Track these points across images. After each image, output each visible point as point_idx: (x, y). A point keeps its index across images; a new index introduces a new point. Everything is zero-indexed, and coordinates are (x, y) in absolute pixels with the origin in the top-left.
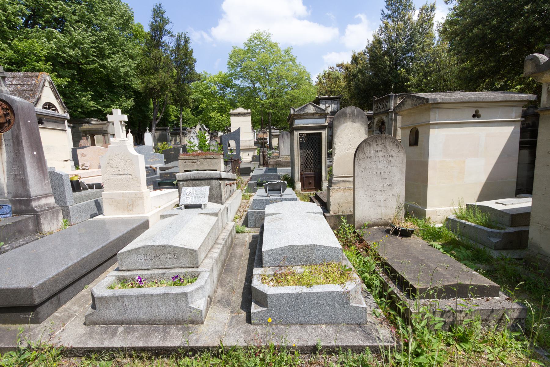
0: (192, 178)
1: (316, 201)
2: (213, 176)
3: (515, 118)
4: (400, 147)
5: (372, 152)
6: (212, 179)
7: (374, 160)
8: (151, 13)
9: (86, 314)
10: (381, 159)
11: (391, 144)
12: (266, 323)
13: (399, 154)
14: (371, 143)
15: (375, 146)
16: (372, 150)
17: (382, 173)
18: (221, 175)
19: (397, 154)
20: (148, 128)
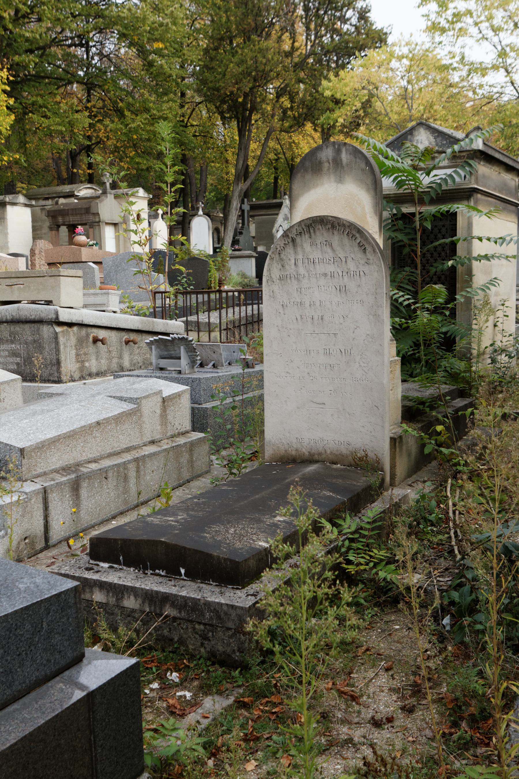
0: (9, 318)
1: (204, 258)
2: (43, 315)
3: (500, 192)
4: (369, 249)
5: (300, 263)
6: (40, 322)
7: (305, 282)
8: (265, 358)
9: (364, 100)
10: (322, 282)
11: (346, 241)
12: (150, 701)
13: (366, 269)
14: (298, 240)
15: (307, 247)
16: (300, 257)
17: (325, 318)
18: (57, 313)
19: (361, 268)
20: (191, 271)
